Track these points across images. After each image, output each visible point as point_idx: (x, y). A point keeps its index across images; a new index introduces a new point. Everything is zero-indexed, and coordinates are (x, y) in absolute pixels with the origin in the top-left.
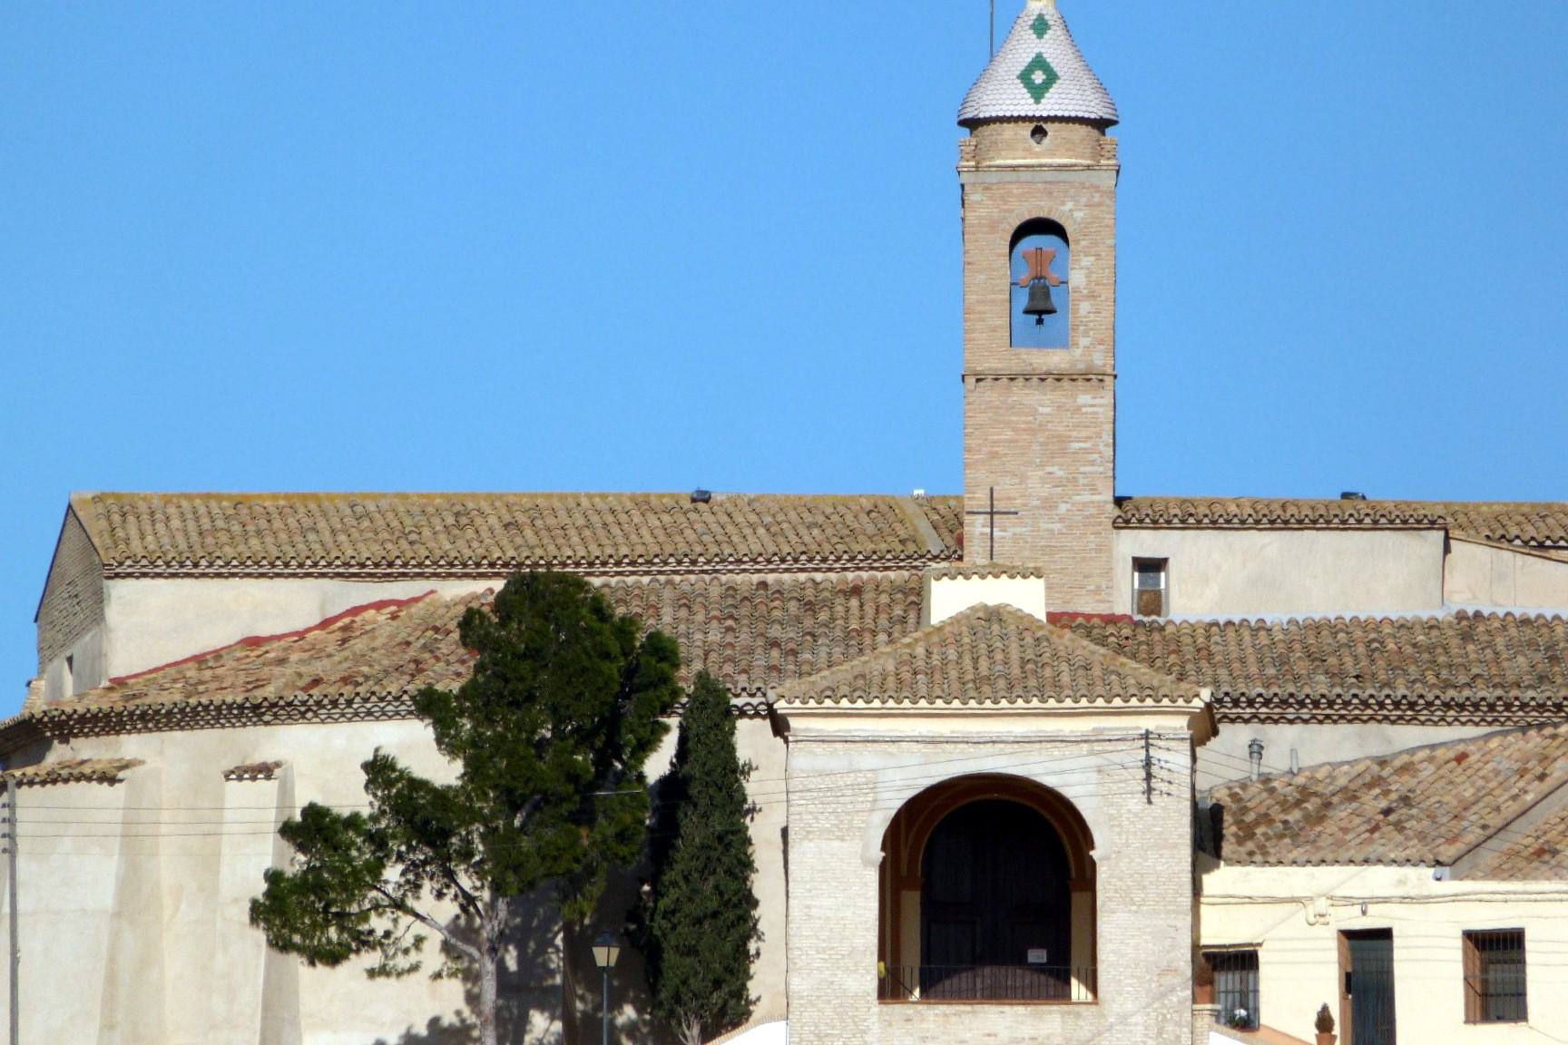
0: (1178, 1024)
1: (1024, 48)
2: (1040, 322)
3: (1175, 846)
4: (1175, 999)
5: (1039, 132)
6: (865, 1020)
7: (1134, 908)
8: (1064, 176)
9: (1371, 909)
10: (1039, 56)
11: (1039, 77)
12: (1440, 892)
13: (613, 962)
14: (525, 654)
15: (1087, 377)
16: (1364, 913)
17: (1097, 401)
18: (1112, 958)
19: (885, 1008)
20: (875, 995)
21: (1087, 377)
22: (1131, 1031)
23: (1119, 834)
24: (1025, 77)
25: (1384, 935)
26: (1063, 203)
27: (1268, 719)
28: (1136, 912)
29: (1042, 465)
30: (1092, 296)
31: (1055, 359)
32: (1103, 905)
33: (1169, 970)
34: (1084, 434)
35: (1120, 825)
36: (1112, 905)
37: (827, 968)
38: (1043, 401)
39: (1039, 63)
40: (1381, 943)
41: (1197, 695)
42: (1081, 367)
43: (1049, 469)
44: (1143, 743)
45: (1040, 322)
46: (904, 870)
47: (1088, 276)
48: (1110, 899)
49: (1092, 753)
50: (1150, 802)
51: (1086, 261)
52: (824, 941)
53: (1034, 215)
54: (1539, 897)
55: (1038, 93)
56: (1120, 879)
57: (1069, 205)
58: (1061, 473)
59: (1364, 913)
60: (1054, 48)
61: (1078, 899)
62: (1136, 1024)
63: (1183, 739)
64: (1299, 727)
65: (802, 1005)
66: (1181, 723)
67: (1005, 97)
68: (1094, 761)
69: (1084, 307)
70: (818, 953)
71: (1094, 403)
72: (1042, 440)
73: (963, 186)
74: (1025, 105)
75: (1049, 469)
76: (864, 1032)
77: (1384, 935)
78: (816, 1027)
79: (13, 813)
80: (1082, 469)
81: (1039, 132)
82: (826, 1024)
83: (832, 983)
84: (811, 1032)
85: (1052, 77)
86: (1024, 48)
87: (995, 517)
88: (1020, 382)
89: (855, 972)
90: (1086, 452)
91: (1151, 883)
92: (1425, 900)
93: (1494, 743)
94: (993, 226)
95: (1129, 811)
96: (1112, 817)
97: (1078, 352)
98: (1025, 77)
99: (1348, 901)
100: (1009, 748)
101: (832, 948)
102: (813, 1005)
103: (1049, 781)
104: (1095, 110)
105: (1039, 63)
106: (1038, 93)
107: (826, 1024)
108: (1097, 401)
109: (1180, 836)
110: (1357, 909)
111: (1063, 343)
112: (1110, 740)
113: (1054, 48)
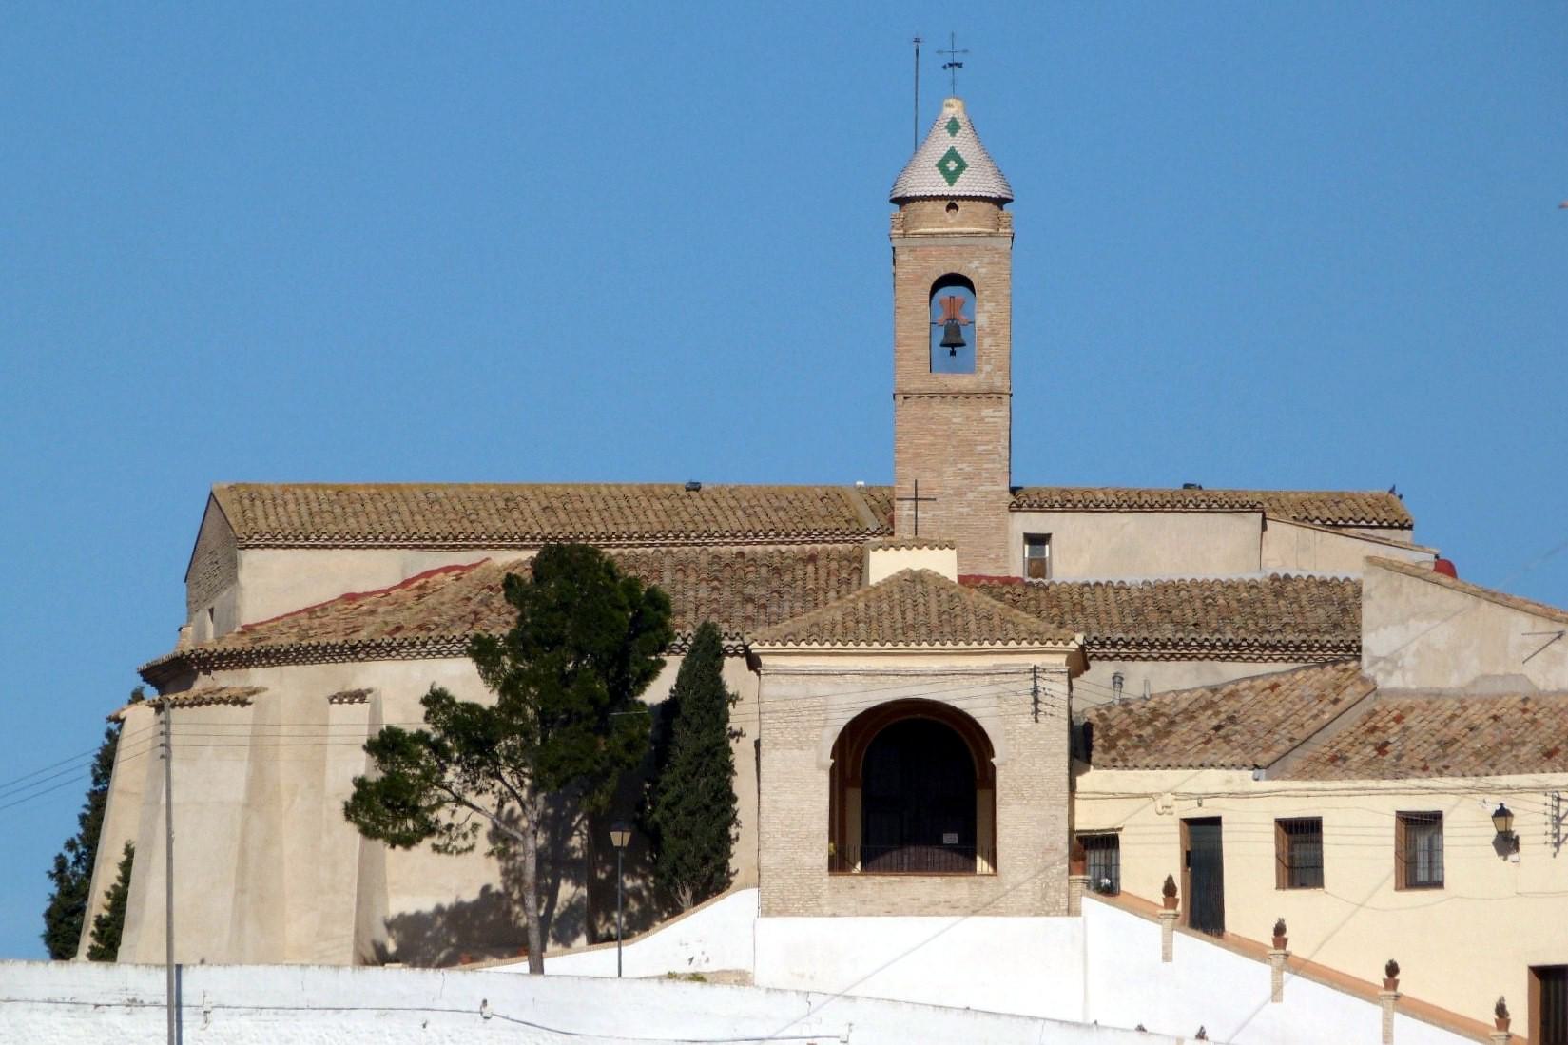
2: (953, 353)
3: (1056, 755)
6: (818, 888)
7: (1025, 802)
9: (1205, 802)
10: (952, 149)
12: (1258, 789)
13: (625, 844)
15: (990, 395)
16: (1200, 805)
18: (1008, 840)
20: (827, 867)
21: (990, 395)
23: (1014, 746)
30: (993, 333)
31: (965, 382)
32: (1002, 799)
33: (1052, 849)
38: (956, 414)
39: (952, 154)
42: (985, 387)
43: (960, 466)
45: (953, 353)
48: (1006, 795)
49: (992, 683)
50: (1037, 721)
55: (951, 178)
56: (1014, 780)
57: (976, 264)
59: (1200, 805)
60: (964, 144)
61: (981, 796)
62: (1027, 891)
63: (1062, 673)
66: (1062, 659)
67: (935, 184)
69: (987, 341)
70: (783, 835)
71: (994, 415)
72: (954, 443)
74: (943, 188)
75: (960, 466)
76: (817, 897)
79: (168, 728)
80: (986, 466)
85: (962, 166)
86: (941, 143)
90: (990, 452)
92: (1247, 795)
93: (1300, 675)
94: (918, 280)
96: (1008, 733)
97: (982, 376)
99: (1189, 796)
100: (929, 680)
101: (793, 833)
102: (780, 877)
103: (959, 705)
104: (996, 190)
105: (952, 154)
106: (951, 178)
109: (1061, 747)
110: (1195, 802)
111: (971, 369)
113: (964, 144)
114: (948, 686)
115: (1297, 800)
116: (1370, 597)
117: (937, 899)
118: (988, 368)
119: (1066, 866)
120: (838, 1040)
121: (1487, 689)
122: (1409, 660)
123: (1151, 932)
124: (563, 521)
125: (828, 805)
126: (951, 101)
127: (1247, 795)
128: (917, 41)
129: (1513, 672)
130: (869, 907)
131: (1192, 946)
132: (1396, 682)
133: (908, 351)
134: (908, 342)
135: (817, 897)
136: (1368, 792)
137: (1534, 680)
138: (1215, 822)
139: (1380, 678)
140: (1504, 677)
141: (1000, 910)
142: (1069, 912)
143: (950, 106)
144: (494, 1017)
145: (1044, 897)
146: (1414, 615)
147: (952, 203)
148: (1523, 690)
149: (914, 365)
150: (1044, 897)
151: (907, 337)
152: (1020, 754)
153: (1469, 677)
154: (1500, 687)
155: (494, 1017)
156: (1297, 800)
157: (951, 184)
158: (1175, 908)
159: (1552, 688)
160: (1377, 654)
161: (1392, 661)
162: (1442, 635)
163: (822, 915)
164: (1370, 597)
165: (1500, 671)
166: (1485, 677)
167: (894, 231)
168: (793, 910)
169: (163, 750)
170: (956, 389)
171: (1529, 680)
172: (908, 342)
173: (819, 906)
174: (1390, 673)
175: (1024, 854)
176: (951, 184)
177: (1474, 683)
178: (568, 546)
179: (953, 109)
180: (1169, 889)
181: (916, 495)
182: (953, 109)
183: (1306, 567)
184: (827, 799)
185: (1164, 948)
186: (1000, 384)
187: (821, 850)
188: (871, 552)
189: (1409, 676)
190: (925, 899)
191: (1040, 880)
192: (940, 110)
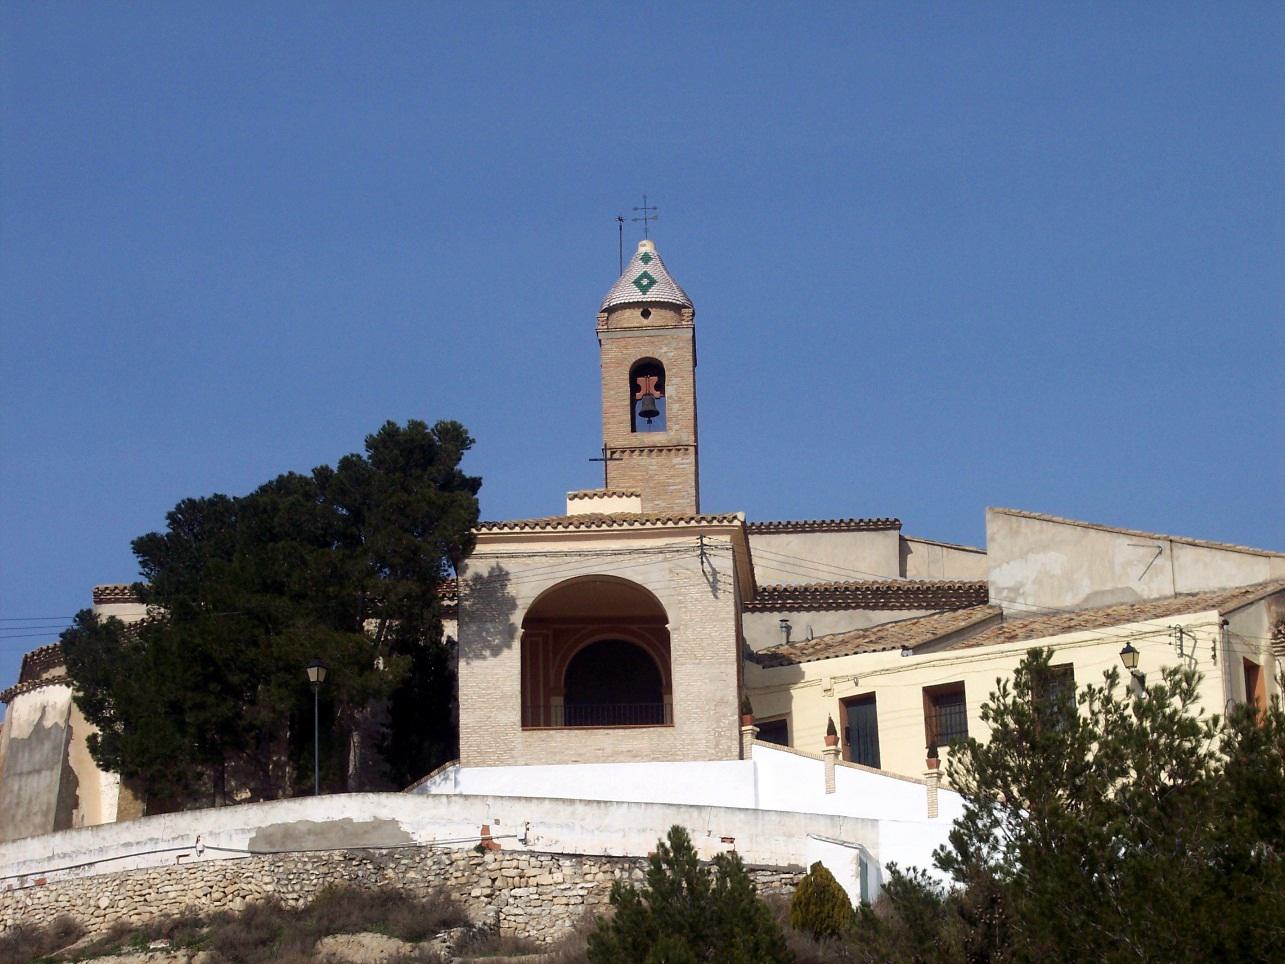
1: (637, 269)
2: (650, 422)
3: (724, 619)
5: (646, 314)
6: (512, 742)
7: (697, 661)
9: (860, 682)
10: (645, 272)
12: (907, 664)
13: (322, 679)
15: (677, 448)
16: (857, 684)
17: (684, 461)
18: (683, 695)
20: (519, 724)
21: (677, 448)
22: (697, 744)
23: (685, 612)
24: (637, 282)
26: (661, 348)
27: (791, 609)
28: (698, 664)
29: (653, 500)
30: (680, 400)
32: (676, 660)
33: (722, 702)
34: (678, 481)
35: (685, 607)
36: (681, 660)
37: (486, 708)
38: (652, 462)
39: (645, 275)
41: (735, 518)
42: (675, 442)
43: (656, 502)
47: (676, 390)
48: (680, 656)
50: (717, 597)
51: (675, 381)
52: (484, 689)
53: (644, 356)
54: (973, 659)
55: (644, 290)
56: (687, 642)
57: (665, 349)
58: (664, 504)
59: (857, 684)
60: (654, 269)
61: (666, 698)
62: (701, 739)
63: (727, 549)
65: (468, 733)
66: (726, 538)
67: (628, 293)
69: (676, 407)
70: (479, 697)
71: (685, 463)
72: (651, 485)
73: (600, 341)
75: (656, 502)
76: (512, 750)
78: (478, 746)
80: (677, 501)
81: (646, 314)
82: (486, 745)
83: (490, 717)
84: (475, 751)
85: (652, 282)
86: (637, 269)
87: (603, 462)
89: (506, 709)
90: (679, 491)
91: (708, 644)
92: (899, 670)
93: (936, 617)
94: (619, 363)
95: (692, 597)
96: (680, 602)
97: (672, 433)
98: (637, 282)
99: (845, 678)
100: (609, 559)
101: (489, 694)
102: (476, 733)
103: (637, 579)
104: (679, 299)
105: (645, 275)
106: (644, 290)
107: (486, 745)
108: (684, 461)
109: (728, 613)
110: (852, 683)
111: (663, 428)
112: (678, 551)
114: (626, 564)
115: (940, 669)
116: (993, 540)
117: (620, 749)
118: (676, 427)
120: (516, 839)
121: (1098, 602)
122: (1029, 588)
124: (504, 862)
125: (520, 669)
126: (644, 242)
127: (899, 670)
128: (621, 220)
129: (1120, 586)
130: (558, 758)
132: (1019, 606)
134: (613, 410)
135: (512, 750)
136: (1004, 654)
137: (1138, 590)
138: (869, 699)
140: (1112, 592)
141: (678, 757)
142: (741, 757)
143: (644, 245)
144: (206, 850)
145: (717, 745)
146: (1031, 550)
147: (646, 309)
148: (1130, 600)
149: (616, 428)
150: (717, 745)
151: (611, 407)
153: (1082, 596)
154: (1108, 600)
155: (206, 850)
156: (940, 669)
159: (1155, 595)
160: (1001, 585)
161: (1016, 591)
162: (1055, 561)
165: (1109, 586)
166: (1096, 594)
167: (600, 327)
170: (651, 444)
171: (1133, 590)
172: (613, 410)
173: (513, 757)
174: (1013, 601)
175: (697, 707)
177: (1087, 599)
179: (646, 247)
180: (831, 730)
181: (601, 460)
182: (646, 247)
183: (936, 576)
184: (518, 664)
186: (686, 439)
187: (514, 714)
188: (568, 500)
189: (1030, 601)
190: (609, 750)
191: (713, 729)
192: (636, 249)
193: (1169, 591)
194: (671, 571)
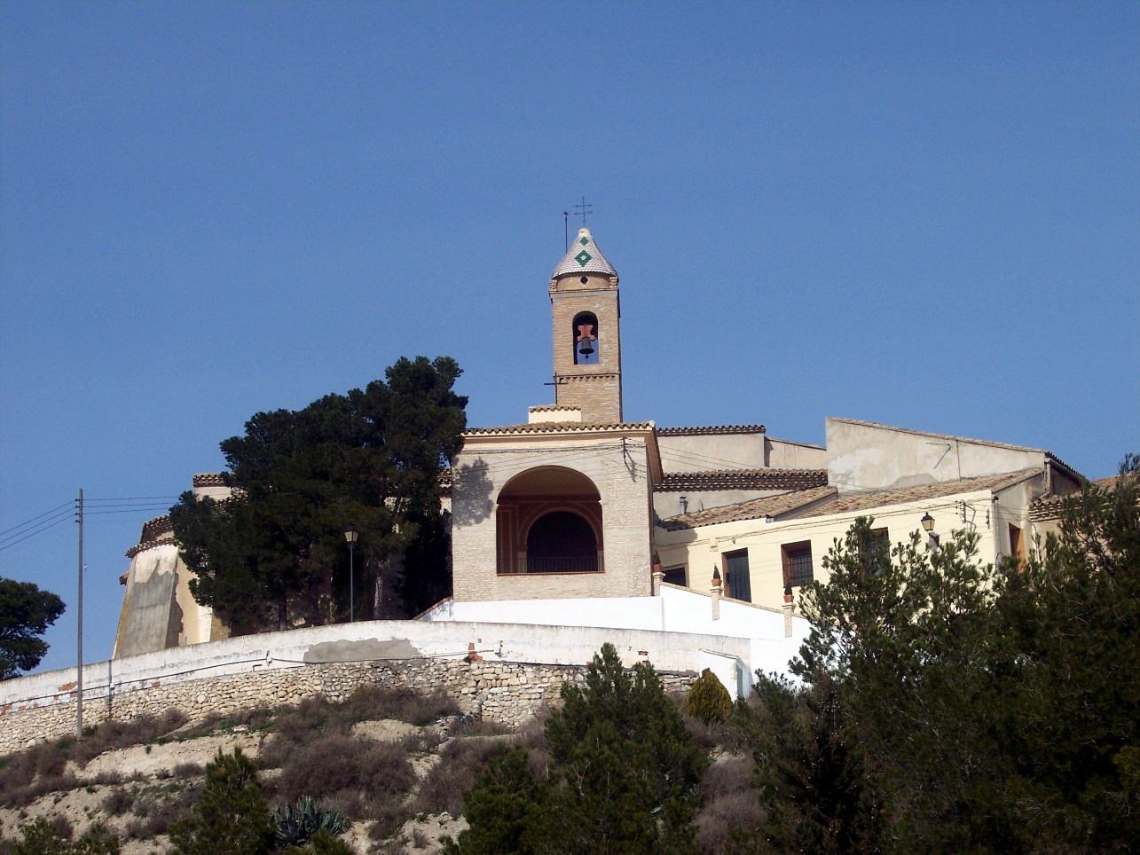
0: (644, 581)
1: (578, 249)
2: (587, 357)
4: (642, 569)
5: (584, 281)
8: (594, 293)
9: (737, 541)
11: (583, 258)
13: (355, 540)
14: (550, 781)
15: (607, 375)
16: (734, 542)
19: (501, 578)
20: (495, 571)
21: (607, 375)
23: (613, 492)
25: (743, 553)
27: (688, 489)
30: (609, 342)
31: (593, 369)
33: (640, 555)
34: (607, 399)
38: (589, 386)
39: (584, 253)
40: (739, 560)
44: (622, 449)
45: (587, 357)
46: (518, 543)
49: (599, 455)
55: (583, 263)
56: (614, 513)
57: (597, 306)
59: (734, 542)
60: (590, 249)
61: (599, 552)
64: (703, 492)
68: (600, 458)
74: (578, 268)
76: (489, 590)
77: (743, 553)
79: (82, 503)
86: (578, 249)
88: (578, 379)
92: (764, 532)
93: (790, 495)
94: (565, 316)
96: (609, 484)
97: (603, 365)
103: (579, 469)
104: (608, 270)
105: (584, 253)
106: (583, 263)
110: (731, 542)
111: (597, 361)
115: (793, 531)
116: (831, 440)
119: (649, 566)
121: (905, 484)
122: (856, 474)
123: (707, 602)
127: (764, 532)
128: (566, 213)
129: (921, 473)
130: (523, 595)
131: (733, 607)
132: (849, 487)
133: (561, 354)
135: (489, 590)
139: (839, 486)
140: (915, 477)
143: (582, 232)
145: (636, 585)
146: (857, 447)
150: (636, 585)
152: (617, 497)
153: (893, 480)
156: (793, 531)
157: (583, 266)
158: (720, 585)
161: (847, 476)
162: (874, 455)
163: (492, 600)
164: (831, 440)
165: (913, 473)
166: (904, 478)
168: (474, 598)
169: (78, 518)
176: (583, 266)
177: (897, 482)
178: (431, 697)
179: (584, 233)
180: (716, 575)
185: (713, 611)
187: (492, 565)
189: (857, 483)
193: (956, 476)
194: (602, 462)
